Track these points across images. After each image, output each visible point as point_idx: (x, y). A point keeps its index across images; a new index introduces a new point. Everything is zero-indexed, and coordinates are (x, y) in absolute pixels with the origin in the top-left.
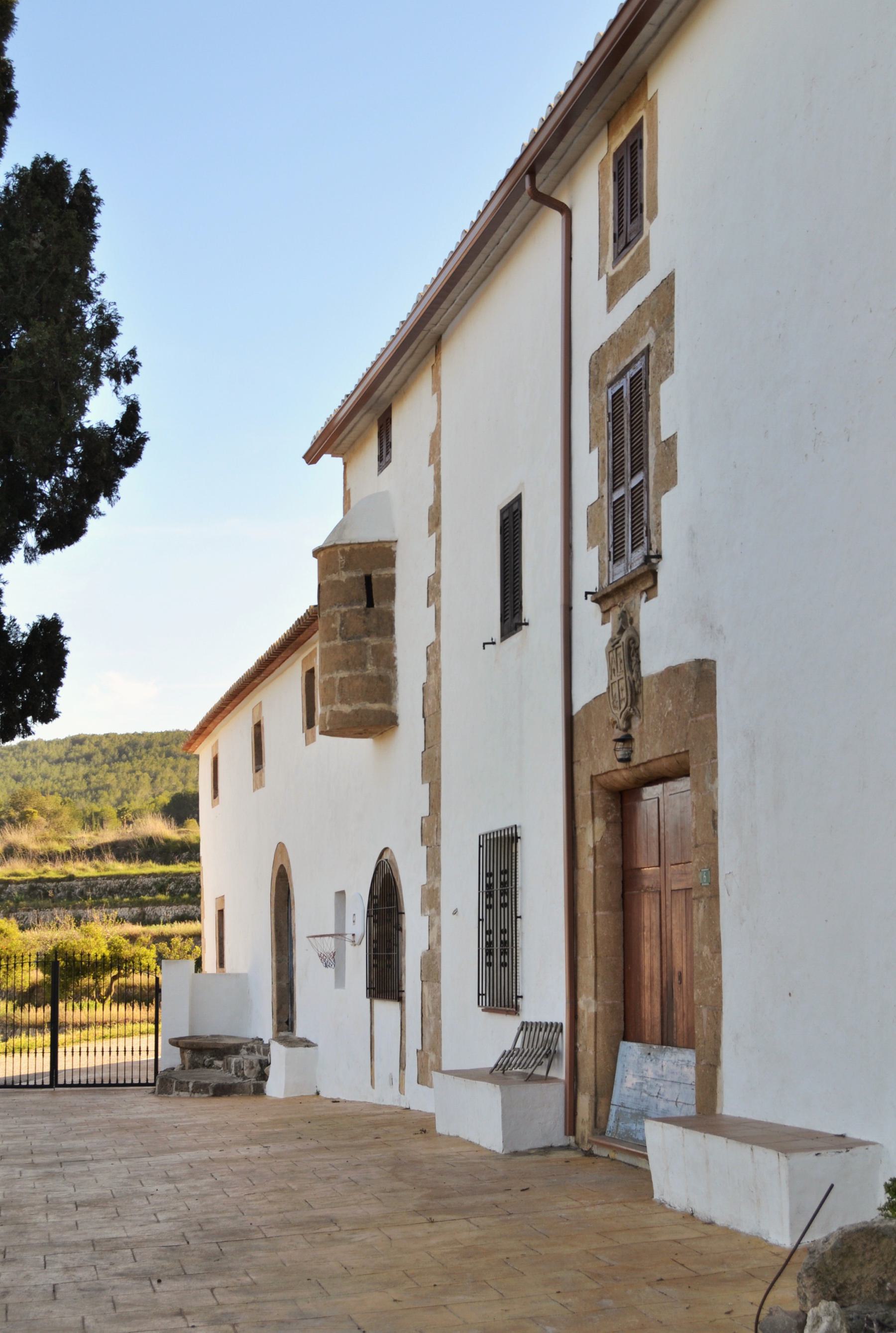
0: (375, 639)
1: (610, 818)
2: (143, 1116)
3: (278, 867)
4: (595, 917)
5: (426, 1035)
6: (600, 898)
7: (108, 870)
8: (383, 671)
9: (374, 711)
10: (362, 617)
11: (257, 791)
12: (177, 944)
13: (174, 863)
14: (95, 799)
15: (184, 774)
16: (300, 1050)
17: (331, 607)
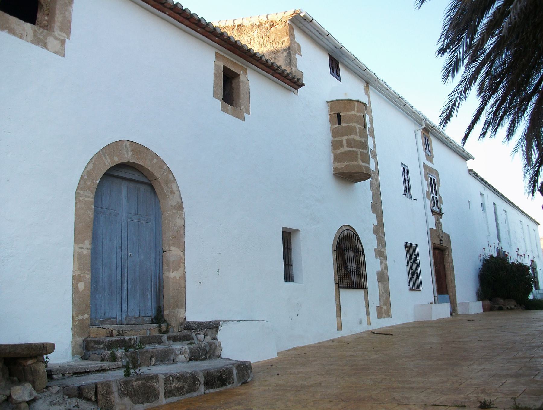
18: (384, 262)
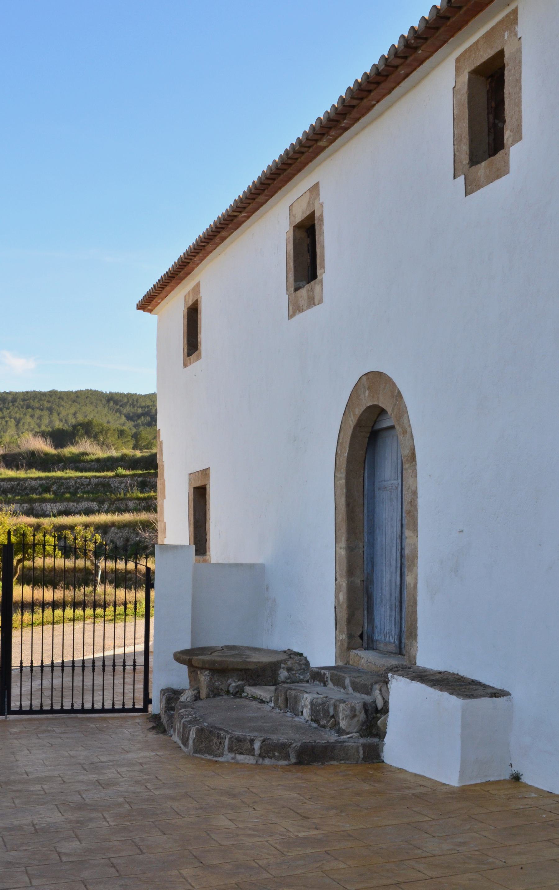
11: (300, 317)
12: (79, 533)
13: (54, 471)
15: (38, 421)
16: (484, 703)
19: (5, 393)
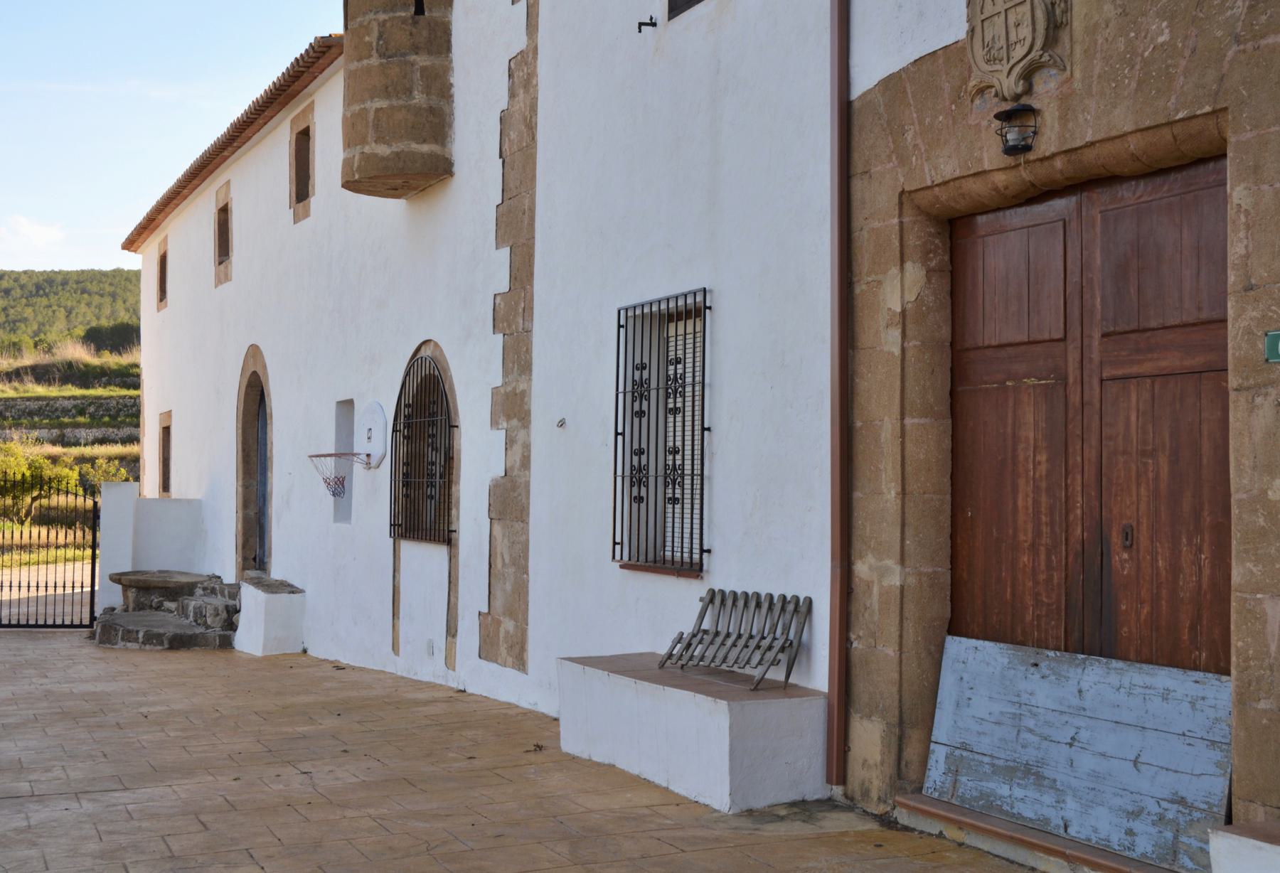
0: (425, 57)
1: (933, 264)
2: (89, 687)
3: (248, 374)
4: (903, 427)
5: (498, 593)
6: (913, 394)
7: (25, 391)
8: (434, 101)
9: (422, 155)
10: (408, 28)
11: (220, 287)
13: (93, 387)
14: (13, 330)
16: (284, 597)
17: (365, 14)
18: (521, 435)
19: (53, 272)
